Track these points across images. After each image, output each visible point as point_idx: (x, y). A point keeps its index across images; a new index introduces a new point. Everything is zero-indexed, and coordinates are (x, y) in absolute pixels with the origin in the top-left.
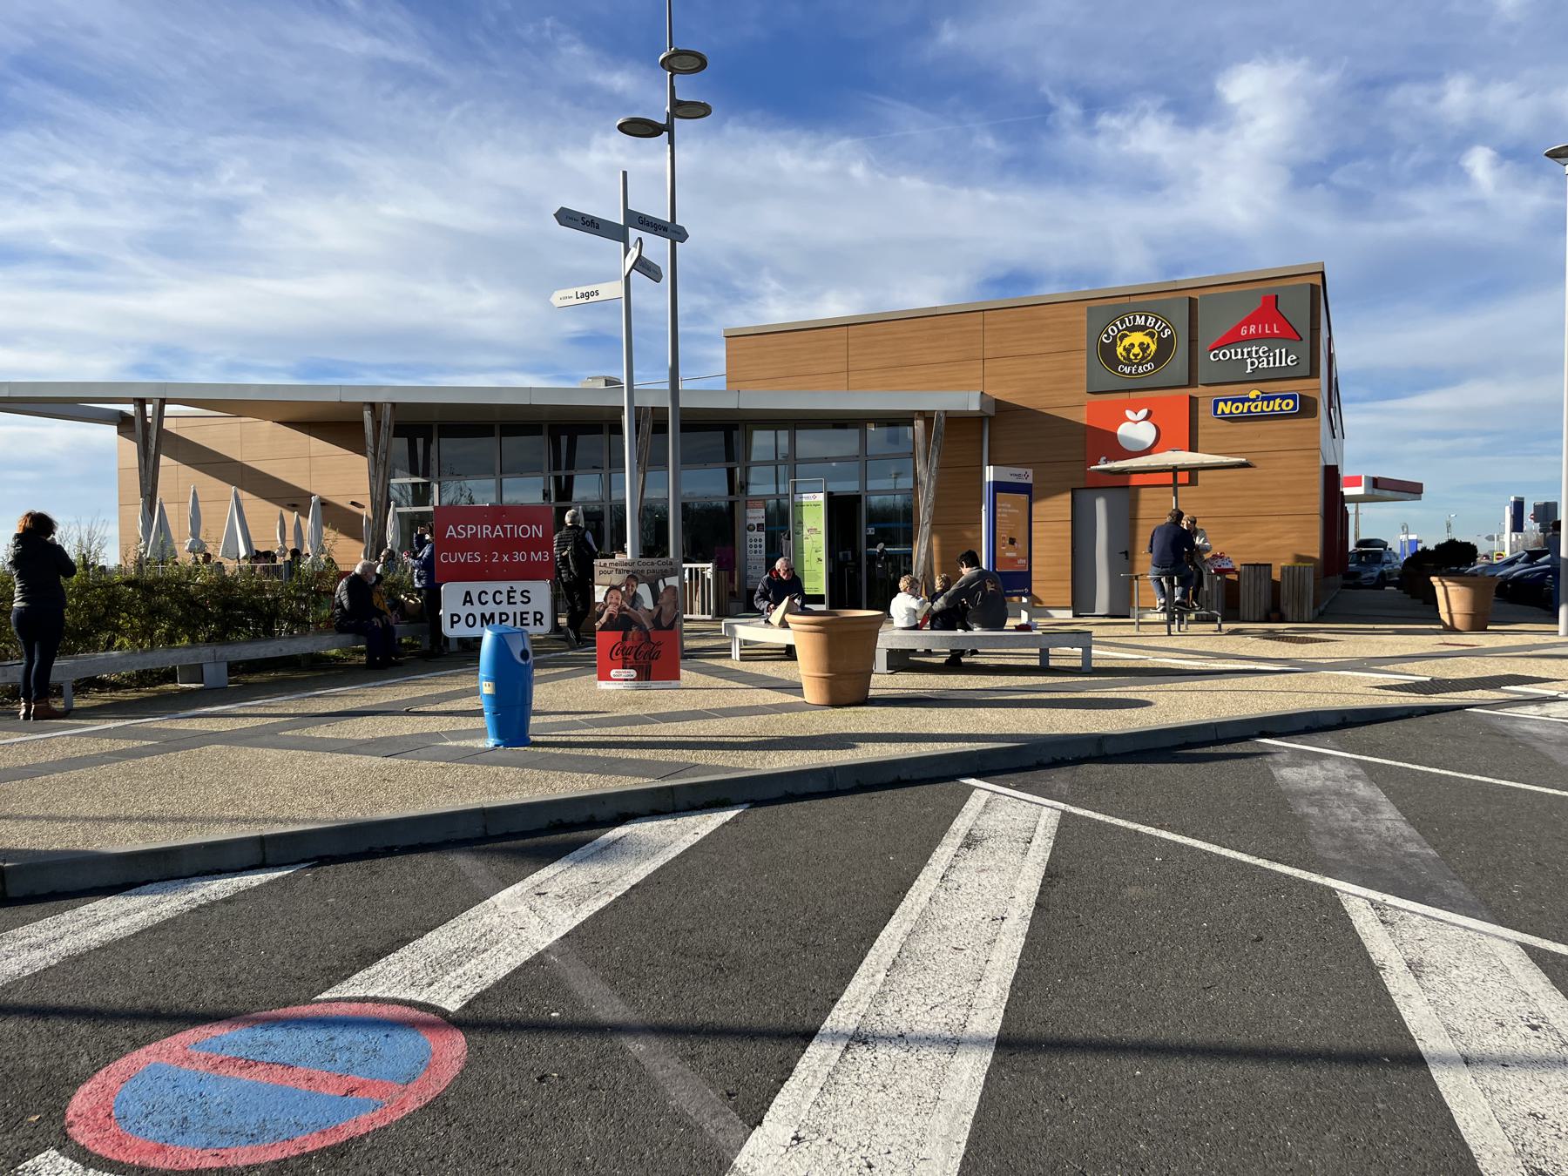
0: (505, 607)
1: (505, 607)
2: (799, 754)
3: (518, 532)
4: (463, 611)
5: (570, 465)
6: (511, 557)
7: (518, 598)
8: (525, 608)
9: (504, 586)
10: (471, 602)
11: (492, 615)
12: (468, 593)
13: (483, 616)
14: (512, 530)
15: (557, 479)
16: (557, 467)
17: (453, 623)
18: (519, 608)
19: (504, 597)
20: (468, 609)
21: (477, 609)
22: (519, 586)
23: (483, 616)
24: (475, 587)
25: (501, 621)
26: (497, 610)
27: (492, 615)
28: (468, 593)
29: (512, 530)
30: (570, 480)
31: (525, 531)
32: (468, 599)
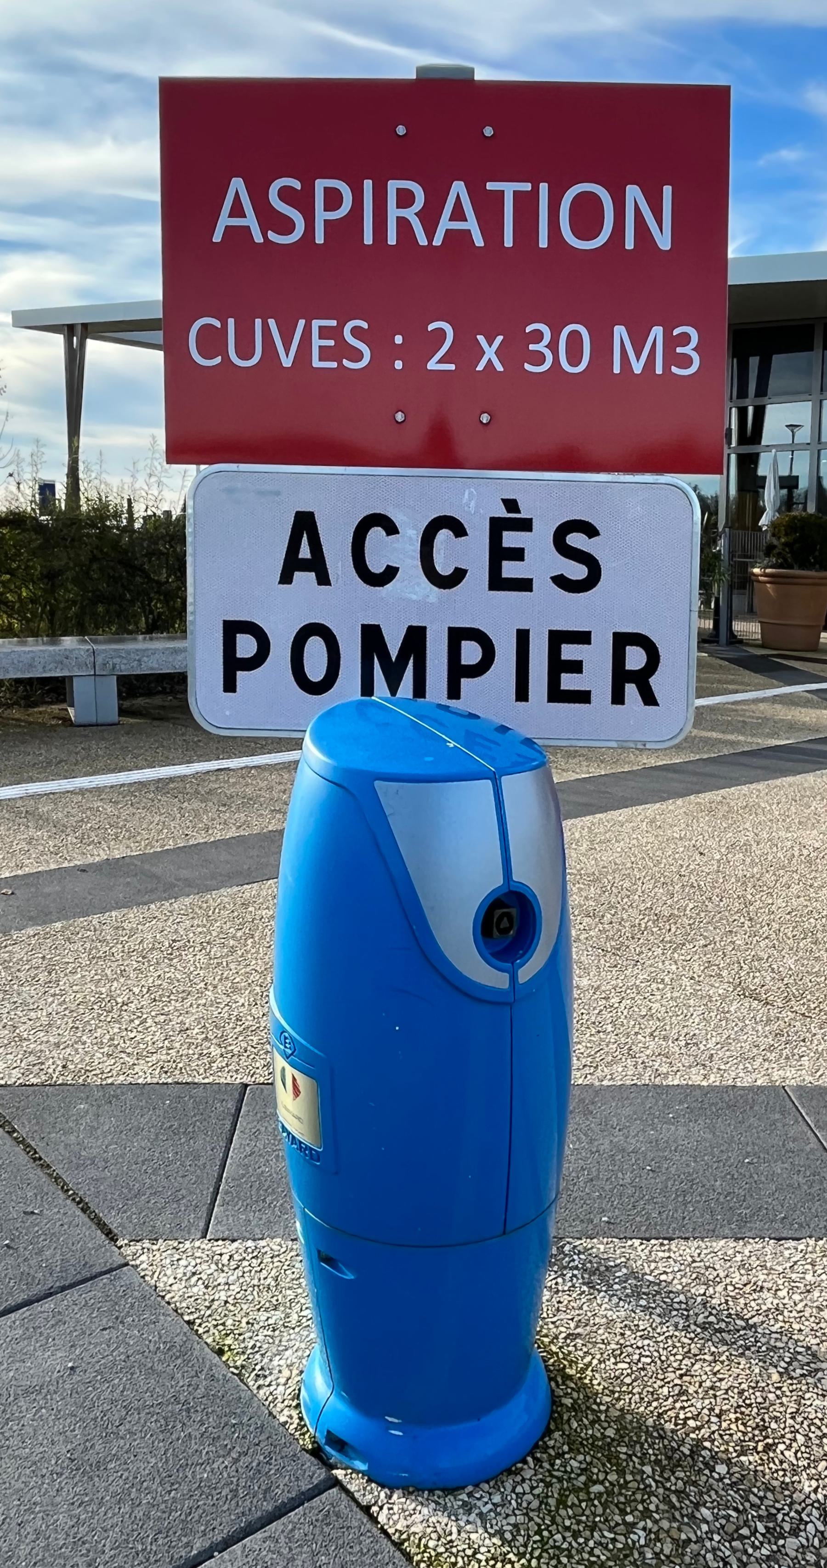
0: (476, 604)
1: (476, 604)
2: (725, 620)
3: (555, 219)
4: (283, 610)
5: (762, 391)
6: (516, 350)
7: (540, 559)
8: (572, 612)
9: (474, 496)
10: (318, 566)
11: (415, 638)
12: (305, 523)
13: (372, 637)
14: (526, 205)
15: (742, 413)
16: (743, 393)
17: (233, 666)
18: (546, 610)
19: (470, 553)
20: (305, 600)
21: (345, 606)
22: (548, 496)
23: (372, 637)
24: (336, 493)
25: (457, 673)
26: (438, 613)
27: (415, 638)
28: (305, 523)
29: (526, 205)
30: (760, 413)
31: (587, 216)
32: (302, 551)
